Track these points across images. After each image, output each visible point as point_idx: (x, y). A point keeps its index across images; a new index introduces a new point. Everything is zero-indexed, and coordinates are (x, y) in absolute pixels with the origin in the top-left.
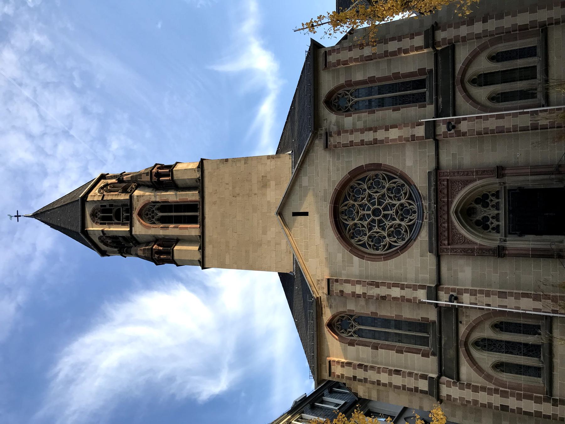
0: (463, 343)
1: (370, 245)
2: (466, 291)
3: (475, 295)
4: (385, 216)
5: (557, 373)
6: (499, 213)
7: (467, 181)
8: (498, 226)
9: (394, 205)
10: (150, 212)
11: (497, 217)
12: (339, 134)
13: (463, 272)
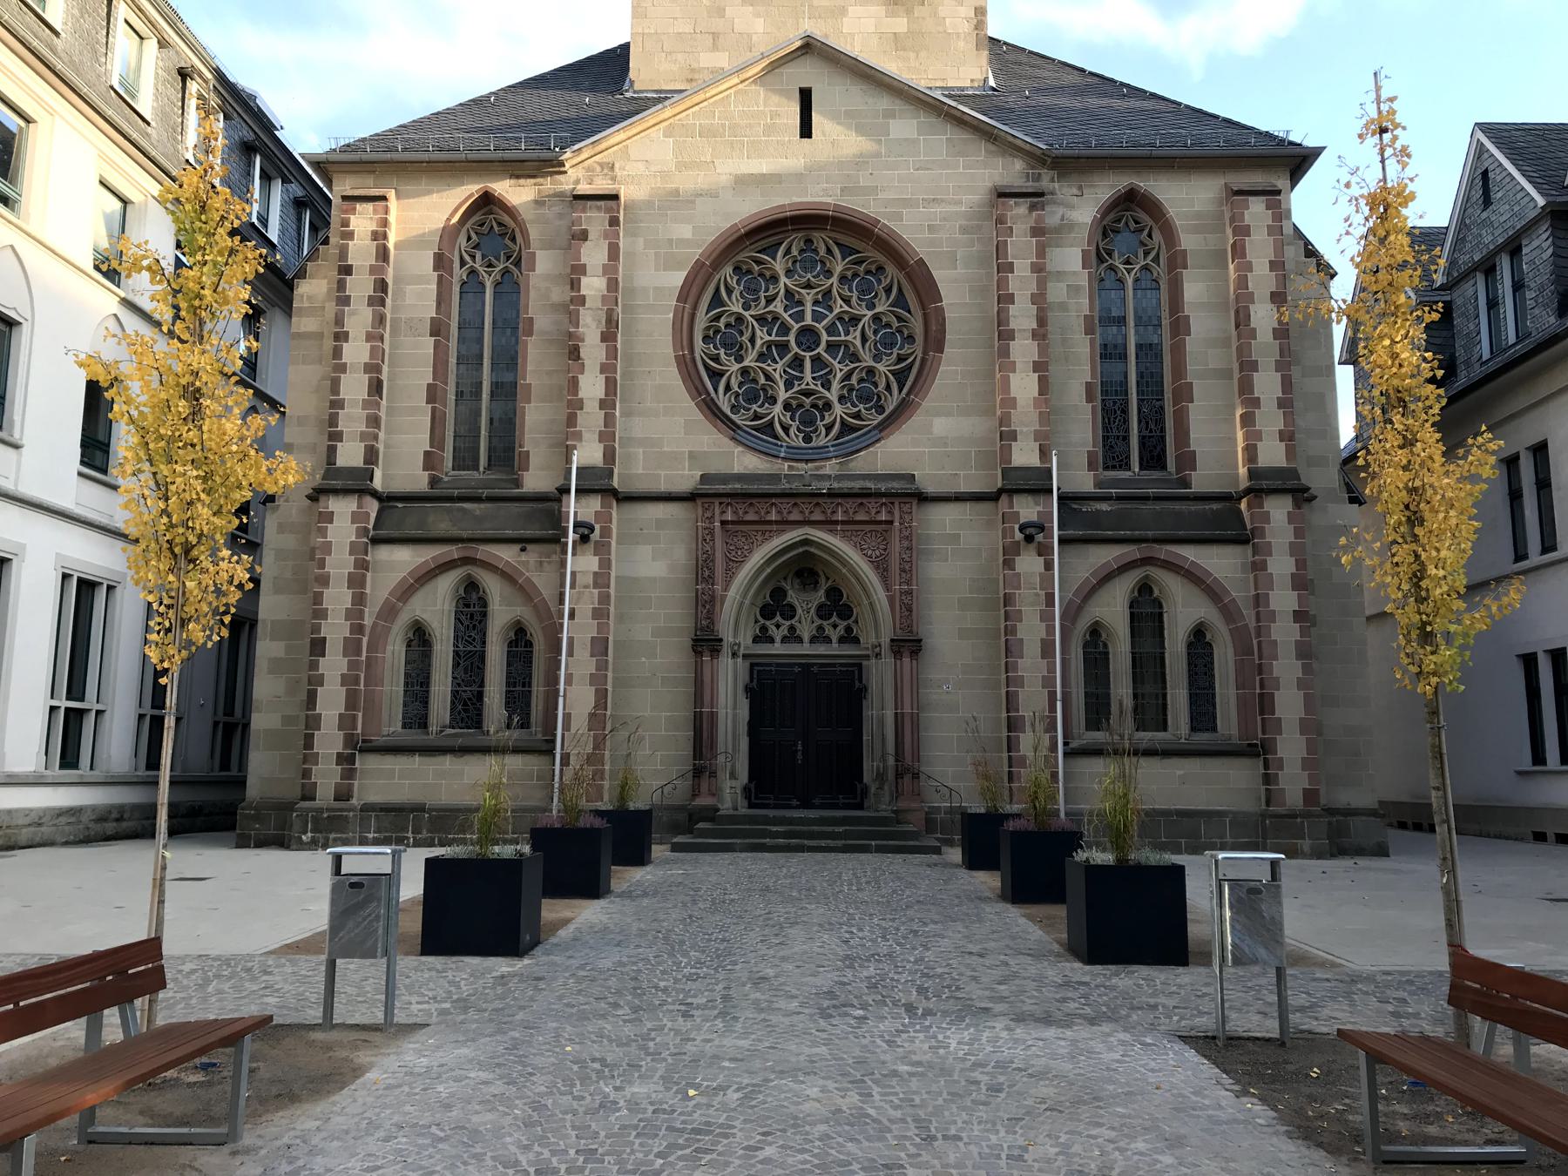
1: (717, 318)
2: (605, 564)
3: (596, 585)
4: (797, 363)
6: (805, 641)
7: (886, 570)
8: (772, 640)
9: (827, 385)
11: (793, 637)
12: (1037, 231)
13: (654, 555)
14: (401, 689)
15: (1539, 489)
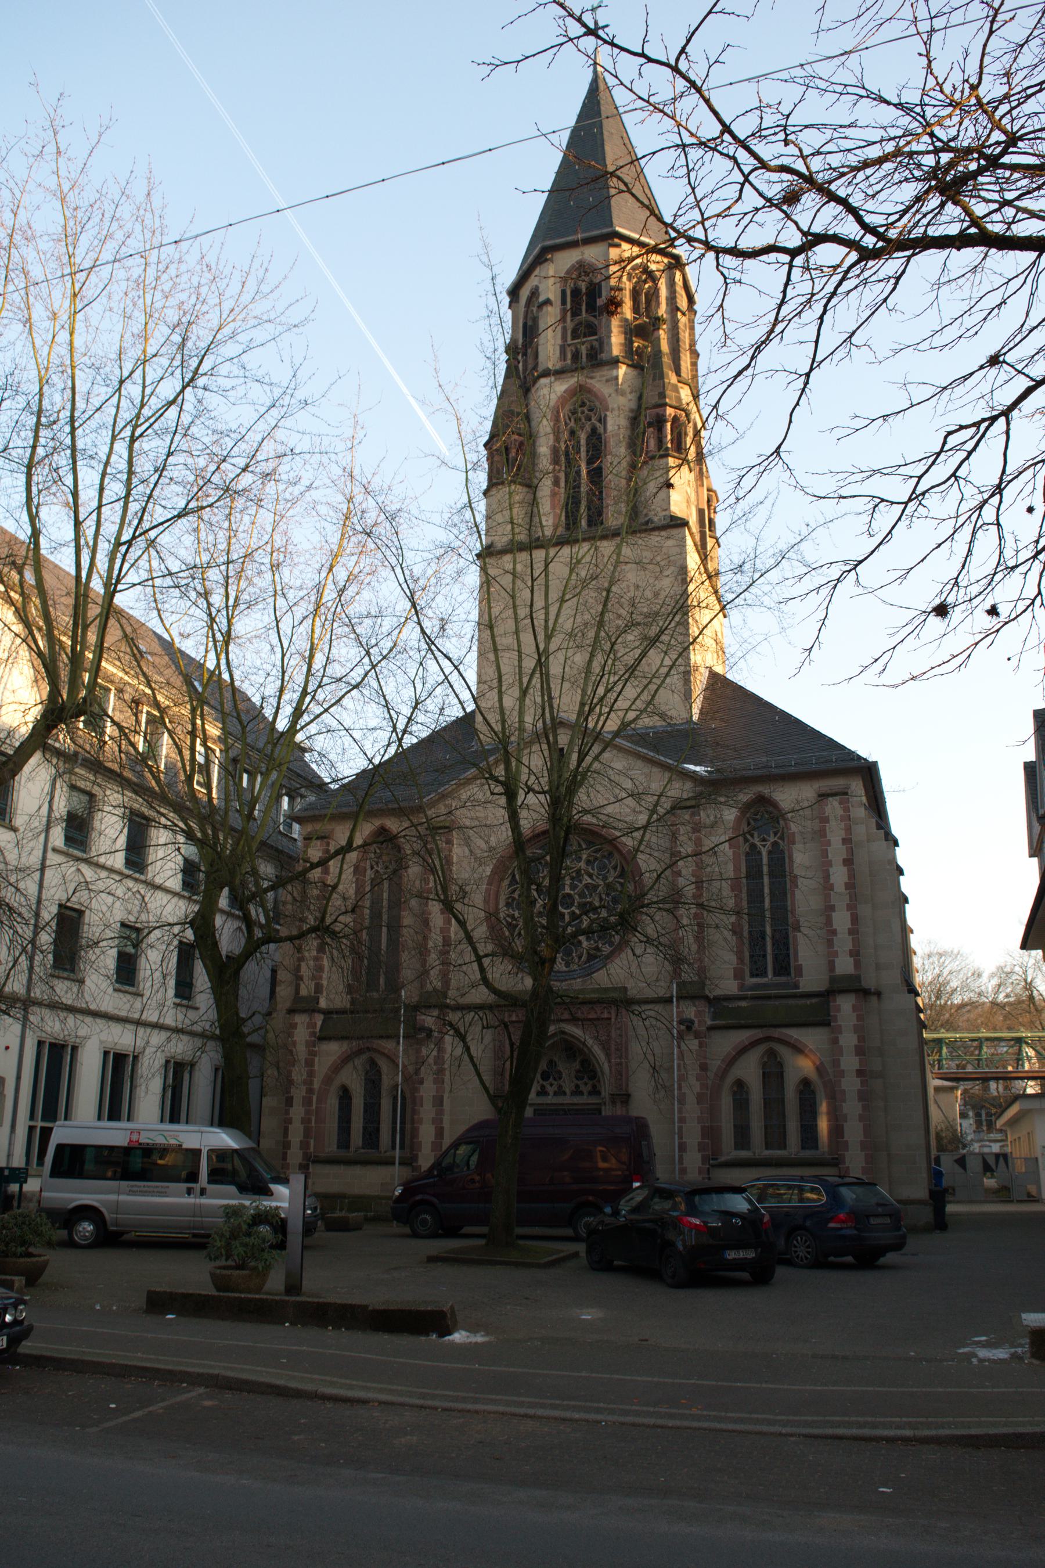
1: (514, 891)
5: (341, 1169)
10: (584, 407)
11: (560, 1092)
14: (336, 1125)
15: (142, 1175)
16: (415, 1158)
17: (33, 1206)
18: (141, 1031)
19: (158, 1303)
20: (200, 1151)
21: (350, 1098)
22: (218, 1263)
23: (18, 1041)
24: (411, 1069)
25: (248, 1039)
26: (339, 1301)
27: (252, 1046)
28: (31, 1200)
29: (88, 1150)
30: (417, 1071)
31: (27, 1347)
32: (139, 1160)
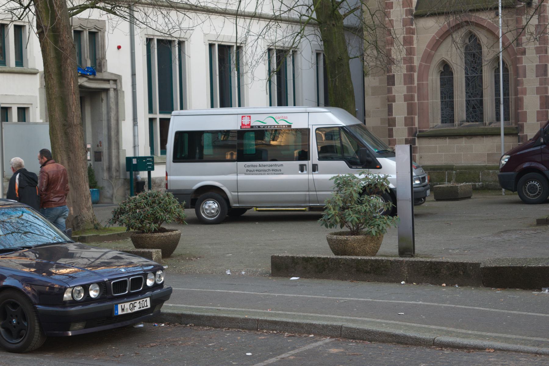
0: (467, 19)
5: (447, 142)
14: (439, 101)
15: (258, 156)
16: (520, 128)
17: (163, 189)
18: (241, 21)
19: (282, 267)
20: (308, 130)
21: (452, 74)
22: (334, 230)
23: (128, 38)
24: (510, 37)
25: (346, 22)
26: (450, 260)
27: (349, 29)
28: (160, 186)
29: (205, 135)
30: (518, 41)
31: (168, 307)
32: (253, 142)
